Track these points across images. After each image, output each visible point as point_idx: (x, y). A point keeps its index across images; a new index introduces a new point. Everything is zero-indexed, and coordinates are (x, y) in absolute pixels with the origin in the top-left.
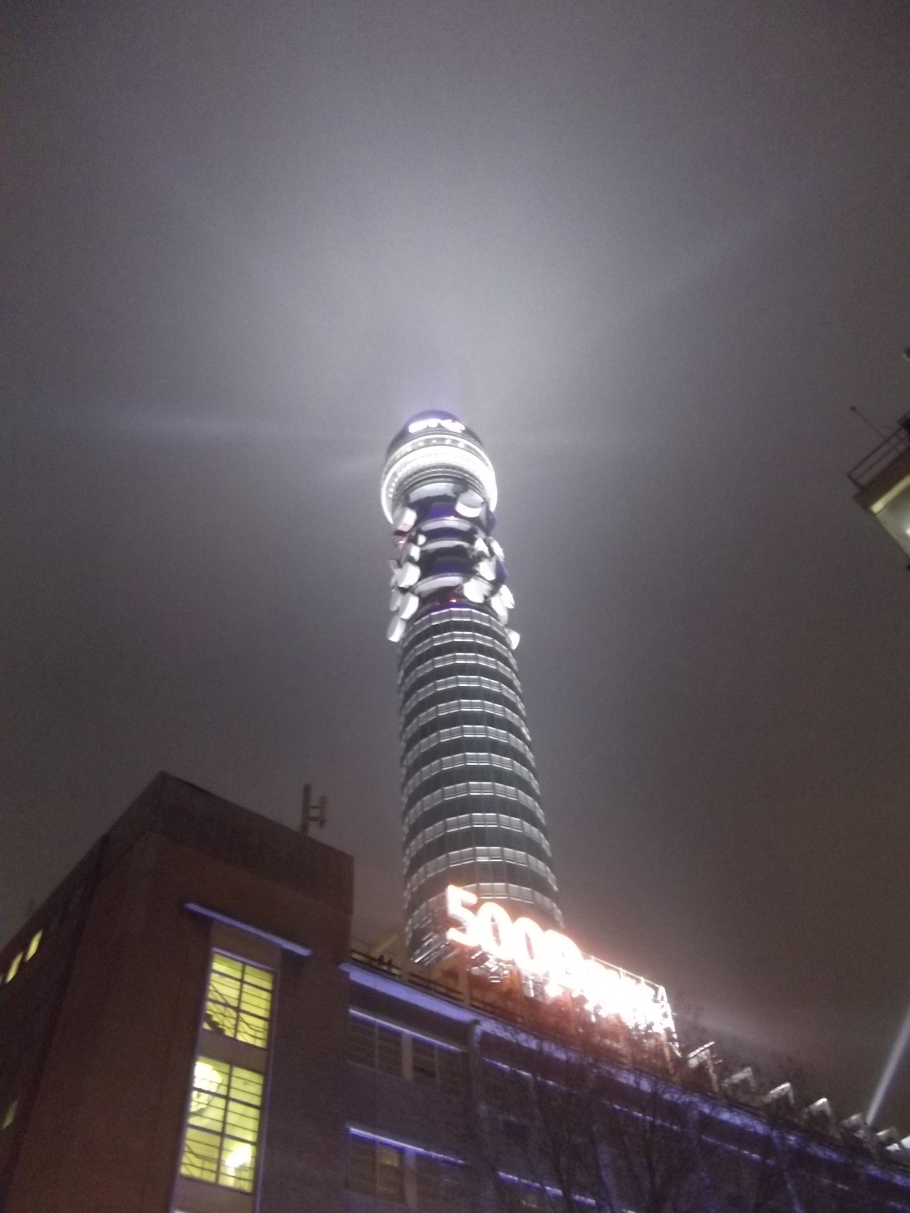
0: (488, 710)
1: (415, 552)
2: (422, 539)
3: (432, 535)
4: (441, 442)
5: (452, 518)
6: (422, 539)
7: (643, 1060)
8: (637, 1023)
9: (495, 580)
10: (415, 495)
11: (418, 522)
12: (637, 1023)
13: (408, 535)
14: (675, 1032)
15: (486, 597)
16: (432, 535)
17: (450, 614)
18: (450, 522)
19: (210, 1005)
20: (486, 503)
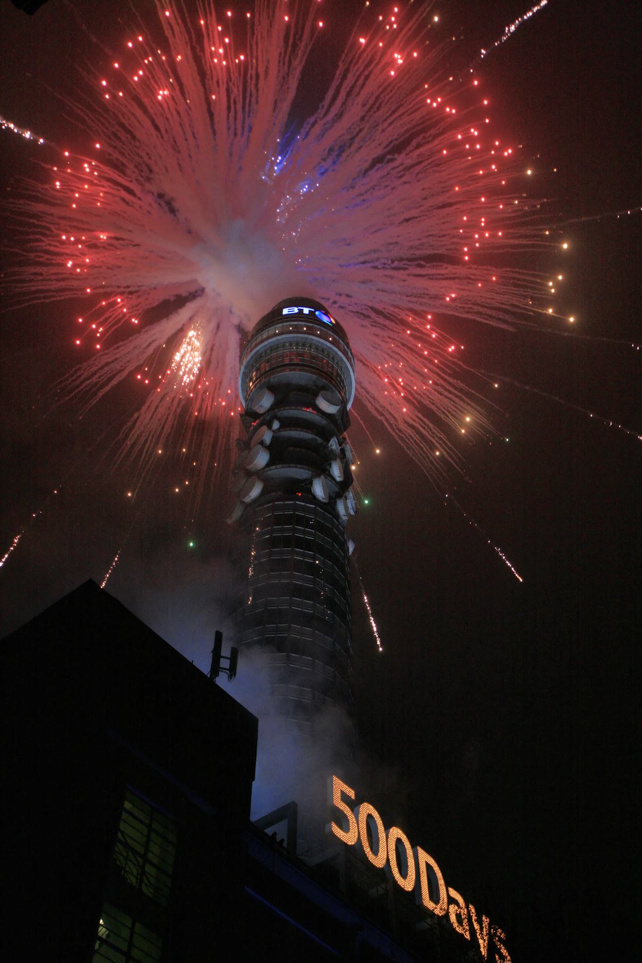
0: (307, 559)
1: (268, 437)
2: (276, 425)
3: (287, 423)
4: (311, 331)
5: (310, 410)
6: (276, 425)
7: (49, 178)
8: (235, 326)
9: (396, 826)
10: (275, 379)
11: (272, 408)
12: (235, 326)
13: (262, 418)
14: (541, 7)
15: (330, 498)
16: (287, 423)
17: (295, 508)
18: (307, 413)
19: (119, 847)
20: (344, 403)
